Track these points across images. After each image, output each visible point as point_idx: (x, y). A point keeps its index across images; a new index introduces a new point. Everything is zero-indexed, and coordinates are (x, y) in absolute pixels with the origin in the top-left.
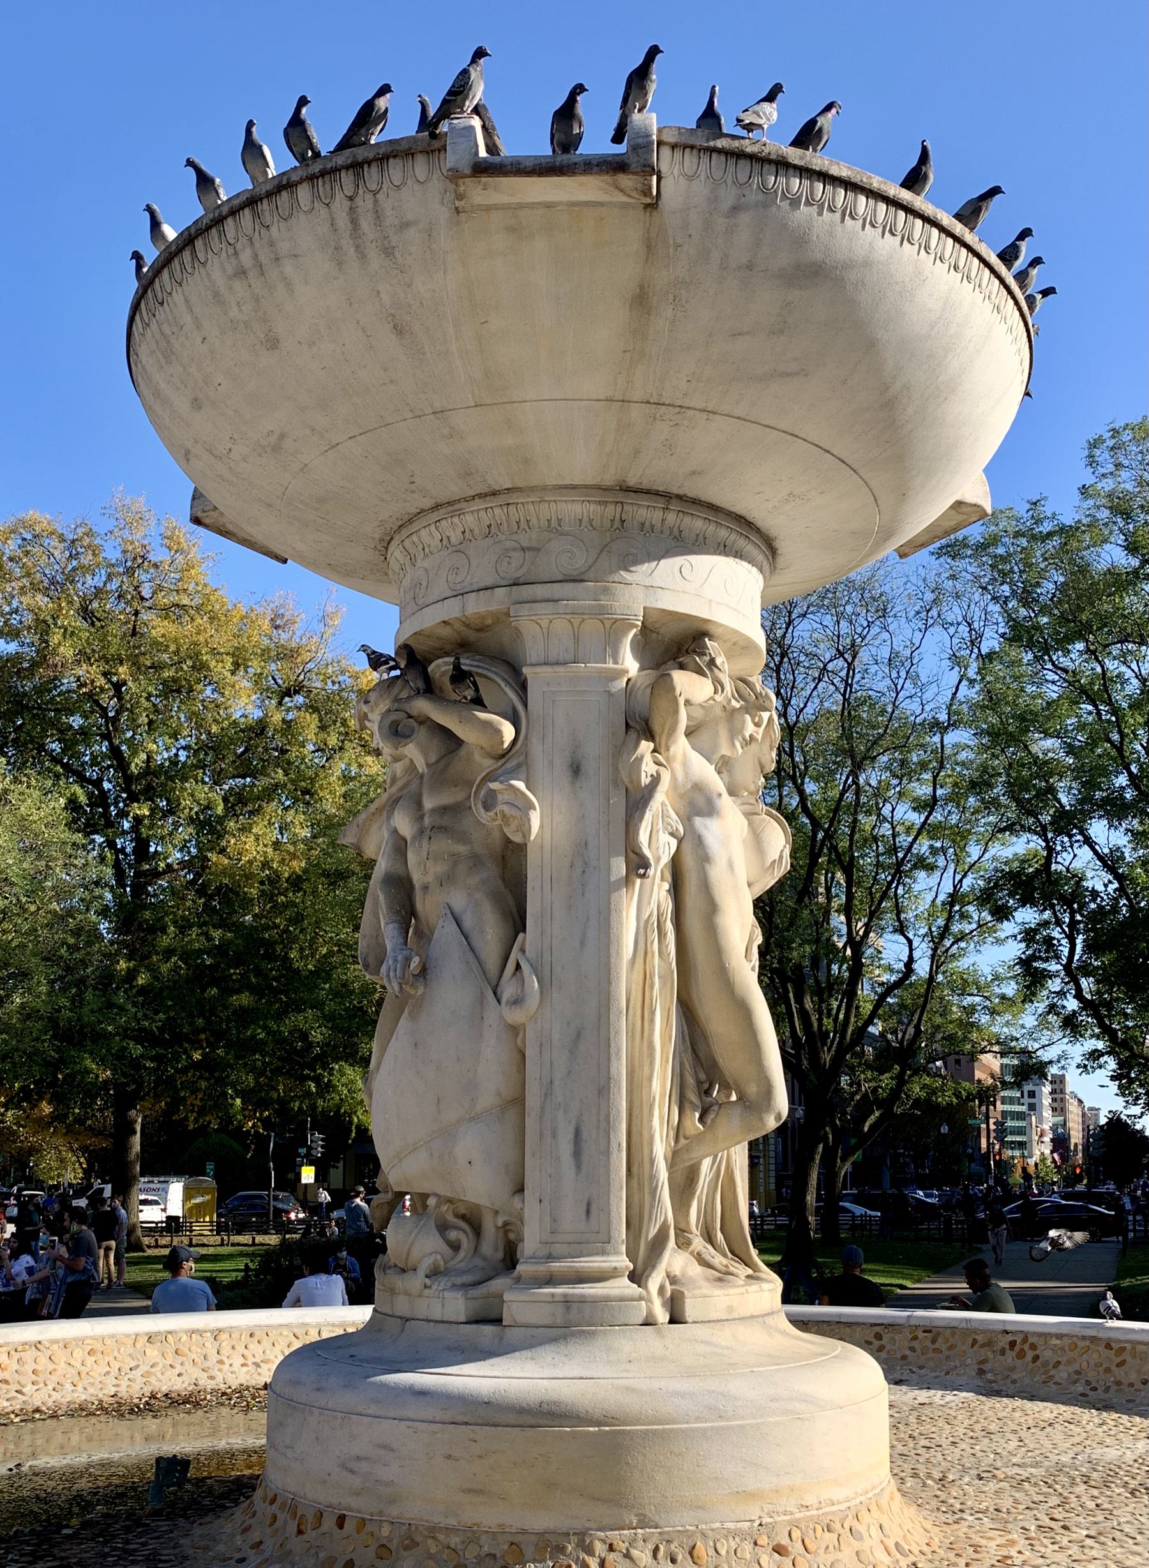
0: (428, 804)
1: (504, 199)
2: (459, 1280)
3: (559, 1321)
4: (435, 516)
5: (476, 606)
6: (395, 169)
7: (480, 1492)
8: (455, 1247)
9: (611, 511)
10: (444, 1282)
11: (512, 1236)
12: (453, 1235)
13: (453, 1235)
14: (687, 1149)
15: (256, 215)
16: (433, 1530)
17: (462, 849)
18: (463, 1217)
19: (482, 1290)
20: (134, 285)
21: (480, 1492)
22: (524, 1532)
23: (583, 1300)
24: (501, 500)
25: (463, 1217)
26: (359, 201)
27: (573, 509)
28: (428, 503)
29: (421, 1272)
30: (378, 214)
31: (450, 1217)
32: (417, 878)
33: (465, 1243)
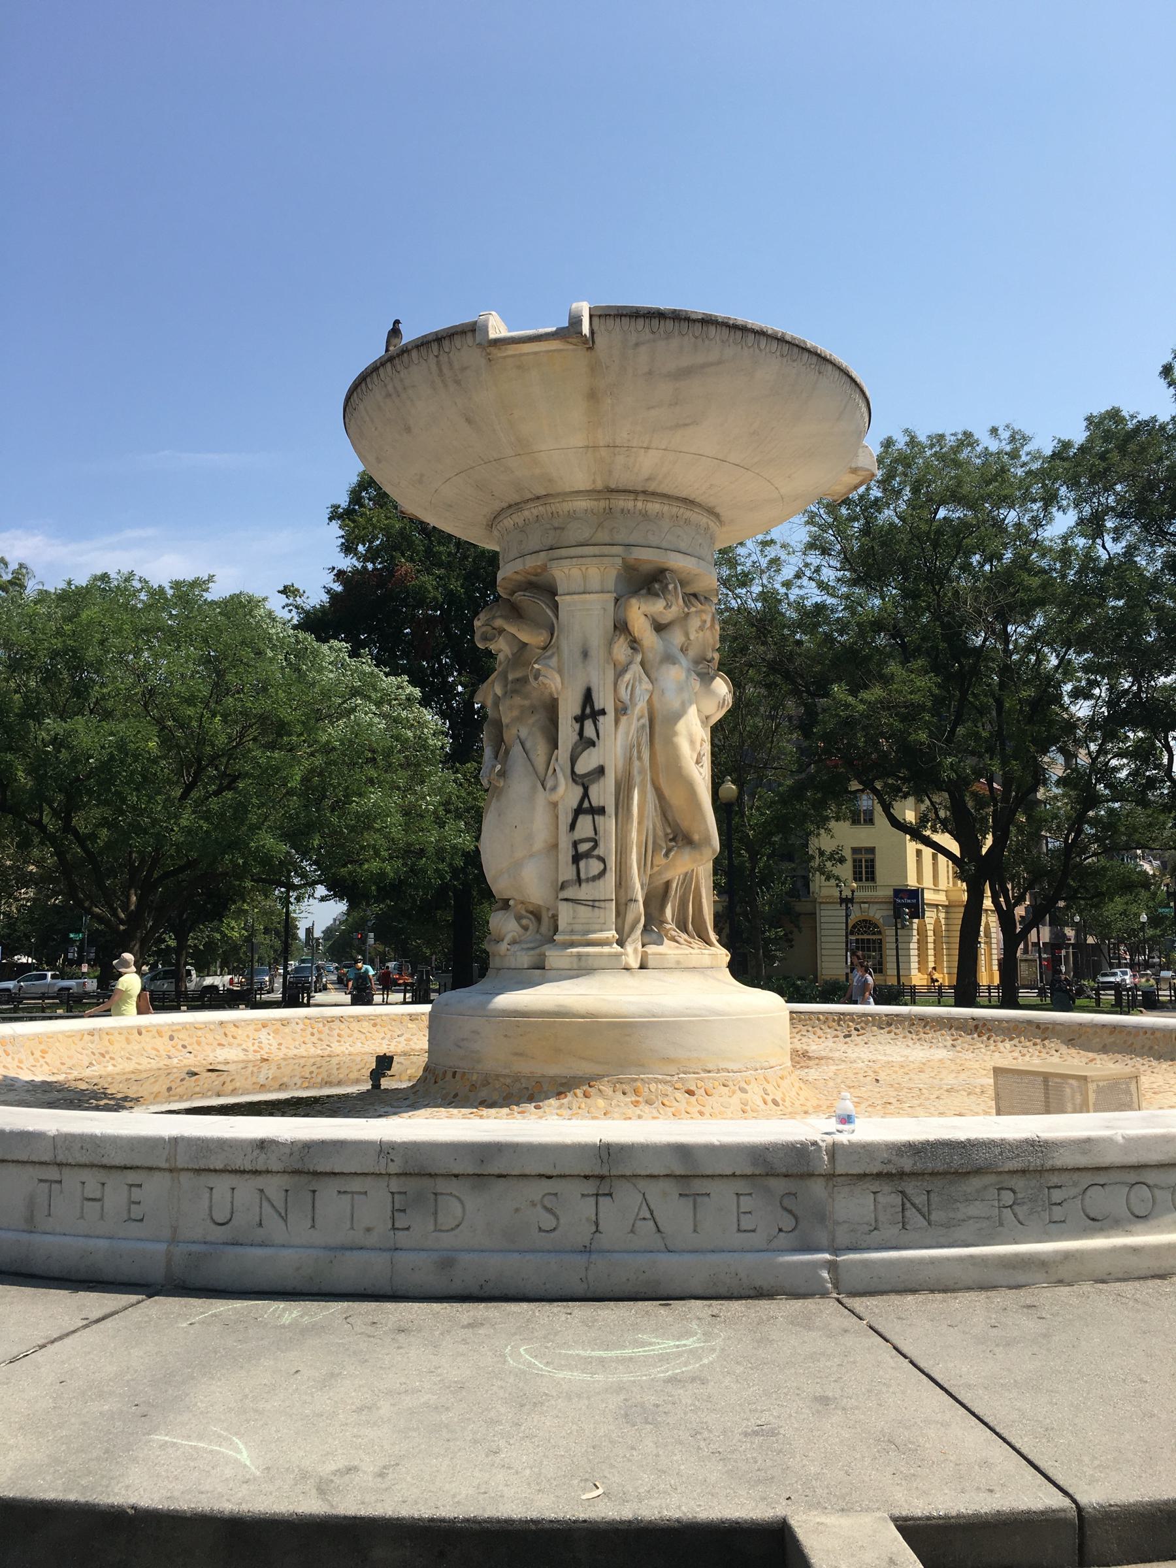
0: (510, 677)
1: (510, 353)
2: (525, 946)
3: (575, 967)
4: (510, 511)
5: (531, 563)
6: (457, 341)
7: (521, 1055)
8: (526, 928)
9: (603, 504)
10: (516, 947)
12: (524, 922)
13: (524, 922)
14: (659, 873)
15: (394, 366)
16: (497, 1076)
17: (527, 703)
18: (531, 913)
19: (538, 951)
20: (377, 350)
21: (521, 1055)
22: (544, 1076)
23: (588, 955)
24: (541, 502)
25: (531, 913)
26: (441, 358)
27: (582, 504)
28: (505, 505)
29: (506, 942)
30: (450, 363)
31: (524, 912)
32: (505, 720)
33: (531, 928)
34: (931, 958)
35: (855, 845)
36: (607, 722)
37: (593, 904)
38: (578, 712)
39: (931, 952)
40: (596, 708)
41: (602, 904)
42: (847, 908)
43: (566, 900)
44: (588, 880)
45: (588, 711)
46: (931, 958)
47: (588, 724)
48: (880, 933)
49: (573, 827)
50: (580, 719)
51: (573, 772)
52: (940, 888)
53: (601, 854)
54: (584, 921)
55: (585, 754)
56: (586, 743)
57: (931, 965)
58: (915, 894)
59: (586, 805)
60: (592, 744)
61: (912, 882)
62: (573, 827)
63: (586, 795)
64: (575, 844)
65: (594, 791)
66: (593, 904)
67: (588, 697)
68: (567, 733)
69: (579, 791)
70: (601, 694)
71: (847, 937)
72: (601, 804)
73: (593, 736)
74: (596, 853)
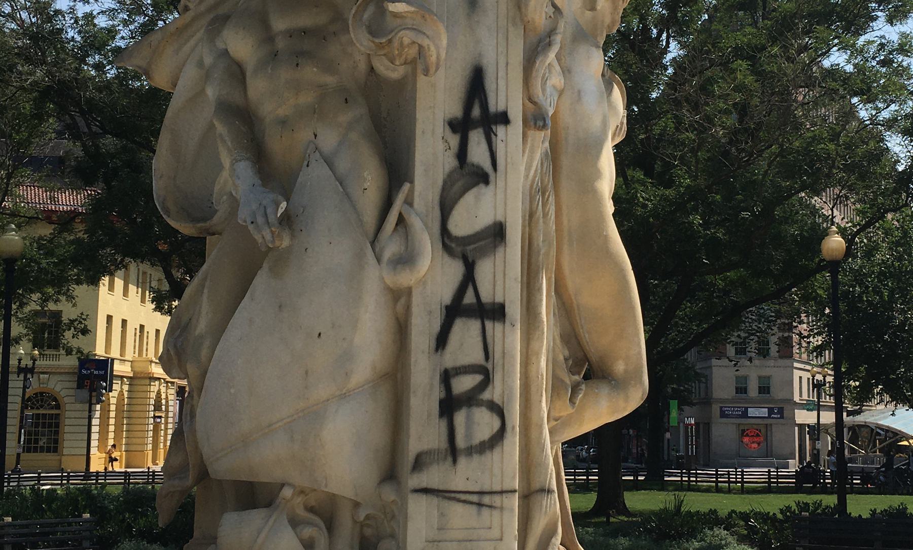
11: (368, 532)
12: (308, 532)
13: (308, 532)
17: (330, 80)
31: (301, 512)
34: (111, 435)
35: (114, 319)
36: (509, 138)
37: (480, 499)
38: (455, 110)
39: (112, 428)
40: (492, 108)
41: (497, 500)
42: (26, 379)
43: (426, 491)
44: (471, 451)
45: (476, 112)
46: (111, 435)
47: (476, 139)
48: (58, 407)
49: (441, 341)
50: (460, 127)
51: (444, 231)
52: (127, 358)
53: (497, 399)
54: (460, 535)
55: (469, 197)
56: (470, 176)
57: (111, 442)
58: (105, 364)
59: (469, 298)
60: (482, 178)
61: (100, 351)
62: (441, 341)
63: (469, 279)
64: (447, 377)
65: (484, 271)
66: (480, 499)
67: (476, 85)
68: (432, 153)
69: (454, 271)
70: (502, 83)
71: (22, 412)
72: (499, 299)
73: (487, 165)
74: (486, 395)
